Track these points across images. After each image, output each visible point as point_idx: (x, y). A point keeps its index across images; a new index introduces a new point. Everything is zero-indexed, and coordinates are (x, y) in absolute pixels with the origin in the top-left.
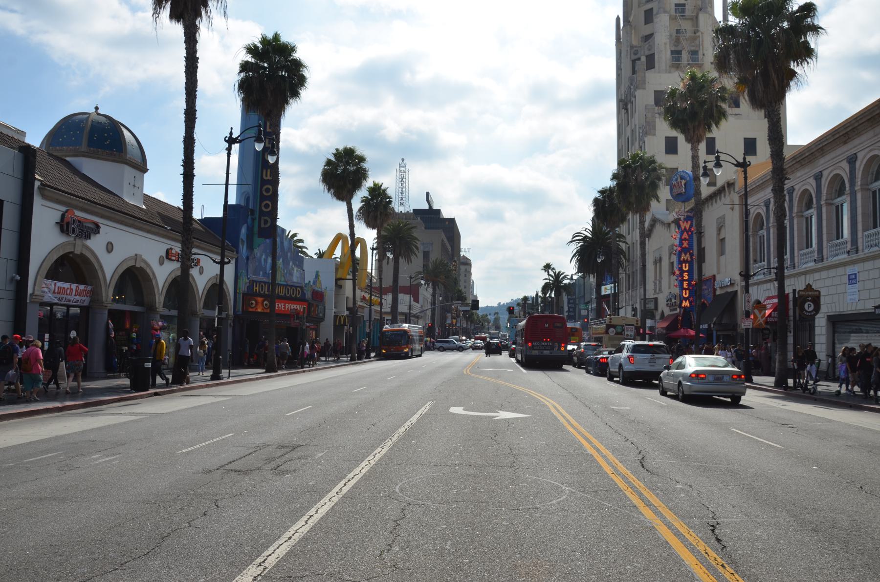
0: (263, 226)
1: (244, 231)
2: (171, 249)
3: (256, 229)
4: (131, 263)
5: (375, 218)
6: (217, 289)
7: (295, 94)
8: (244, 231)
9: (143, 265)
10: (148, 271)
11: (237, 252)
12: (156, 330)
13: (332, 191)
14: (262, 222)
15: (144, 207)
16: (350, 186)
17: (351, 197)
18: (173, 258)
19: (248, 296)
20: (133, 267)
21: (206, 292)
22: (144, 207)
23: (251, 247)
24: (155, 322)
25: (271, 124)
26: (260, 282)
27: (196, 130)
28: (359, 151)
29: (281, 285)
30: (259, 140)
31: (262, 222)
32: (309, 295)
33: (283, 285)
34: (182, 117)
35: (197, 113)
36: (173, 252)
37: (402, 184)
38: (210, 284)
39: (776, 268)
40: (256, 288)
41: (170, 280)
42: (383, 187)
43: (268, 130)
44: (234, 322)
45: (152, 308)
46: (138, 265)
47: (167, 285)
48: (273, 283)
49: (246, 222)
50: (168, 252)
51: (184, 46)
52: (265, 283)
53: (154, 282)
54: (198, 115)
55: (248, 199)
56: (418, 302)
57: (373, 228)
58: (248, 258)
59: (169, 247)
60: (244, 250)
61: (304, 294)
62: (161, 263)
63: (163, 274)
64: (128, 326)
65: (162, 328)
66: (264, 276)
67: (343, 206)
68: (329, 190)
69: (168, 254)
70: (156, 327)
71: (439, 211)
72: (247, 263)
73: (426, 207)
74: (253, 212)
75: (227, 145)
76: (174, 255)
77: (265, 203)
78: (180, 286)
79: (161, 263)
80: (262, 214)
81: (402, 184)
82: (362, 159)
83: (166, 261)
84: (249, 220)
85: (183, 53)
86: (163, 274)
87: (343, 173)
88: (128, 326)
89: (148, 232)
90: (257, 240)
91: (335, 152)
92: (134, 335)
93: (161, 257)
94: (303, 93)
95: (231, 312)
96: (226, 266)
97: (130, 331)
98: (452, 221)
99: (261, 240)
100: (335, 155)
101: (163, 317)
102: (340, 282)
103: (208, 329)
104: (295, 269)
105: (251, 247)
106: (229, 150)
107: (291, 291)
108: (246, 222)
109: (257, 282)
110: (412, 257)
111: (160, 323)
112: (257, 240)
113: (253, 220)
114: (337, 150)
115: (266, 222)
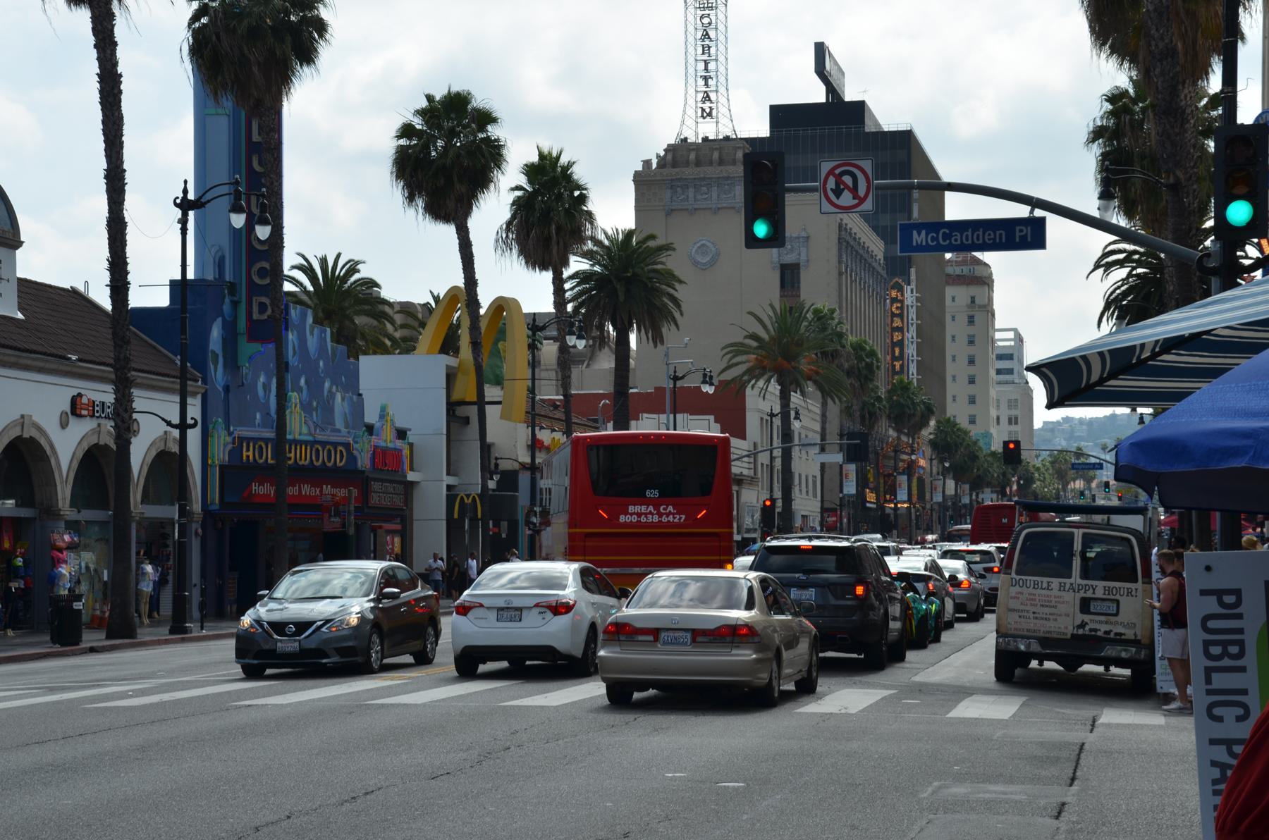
0: (256, 316)
1: (216, 333)
2: (80, 395)
3: (242, 324)
4: (15, 433)
5: (546, 241)
6: (168, 464)
7: (307, 55)
8: (216, 333)
9: (34, 433)
10: (43, 442)
11: (205, 381)
12: (60, 550)
13: (420, 203)
14: (255, 309)
15: (20, 316)
16: (461, 188)
17: (467, 211)
18: (84, 412)
19: (234, 474)
20: (19, 438)
21: (145, 469)
22: (20, 316)
23: (232, 363)
24: (56, 536)
25: (260, 128)
26: (255, 440)
27: (127, 204)
28: (480, 100)
29: (301, 443)
30: (236, 209)
31: (255, 309)
32: (364, 461)
33: (306, 443)
34: (102, 185)
35: (127, 175)
36: (84, 400)
37: (707, 49)
38: (153, 453)
39: (740, 481)
40: (248, 454)
41: (80, 454)
42: (564, 160)
43: (256, 137)
44: (203, 526)
45: (50, 511)
46: (26, 435)
47: (75, 465)
48: (280, 442)
49: (221, 314)
50: (75, 402)
51: (94, 54)
52: (266, 441)
53: (53, 461)
54: (129, 177)
55: (220, 264)
56: (743, 437)
57: (544, 267)
58: (227, 389)
59: (75, 392)
60: (218, 374)
61: (352, 458)
62: (64, 425)
63: (66, 445)
64: (7, 545)
65: (72, 547)
66: (264, 424)
67: (448, 232)
68: (411, 199)
69: (76, 408)
70: (60, 544)
71: (859, 108)
72: (227, 400)
73: (816, 94)
74: (233, 288)
75: (178, 213)
76: (85, 407)
77: (258, 265)
78: (101, 466)
79: (64, 425)
80: (253, 289)
81: (707, 49)
82: (486, 118)
83: (72, 420)
84: (227, 307)
85: (95, 68)
86: (66, 445)
87: (444, 156)
88: (7, 545)
89: (40, 370)
90: (247, 349)
91: (424, 103)
92: (19, 562)
93: (63, 414)
94: (326, 53)
95: (197, 507)
96: (189, 431)
97: (11, 554)
98: (905, 140)
99: (255, 347)
100: (421, 113)
101: (72, 526)
102: (461, 411)
103: (157, 542)
104: (339, 397)
105: (232, 363)
106: (183, 222)
107: (323, 455)
108: (221, 314)
109: (248, 440)
110: (664, 330)
111: (67, 538)
112: (247, 349)
113: (235, 304)
114: (429, 98)
115: (262, 308)
